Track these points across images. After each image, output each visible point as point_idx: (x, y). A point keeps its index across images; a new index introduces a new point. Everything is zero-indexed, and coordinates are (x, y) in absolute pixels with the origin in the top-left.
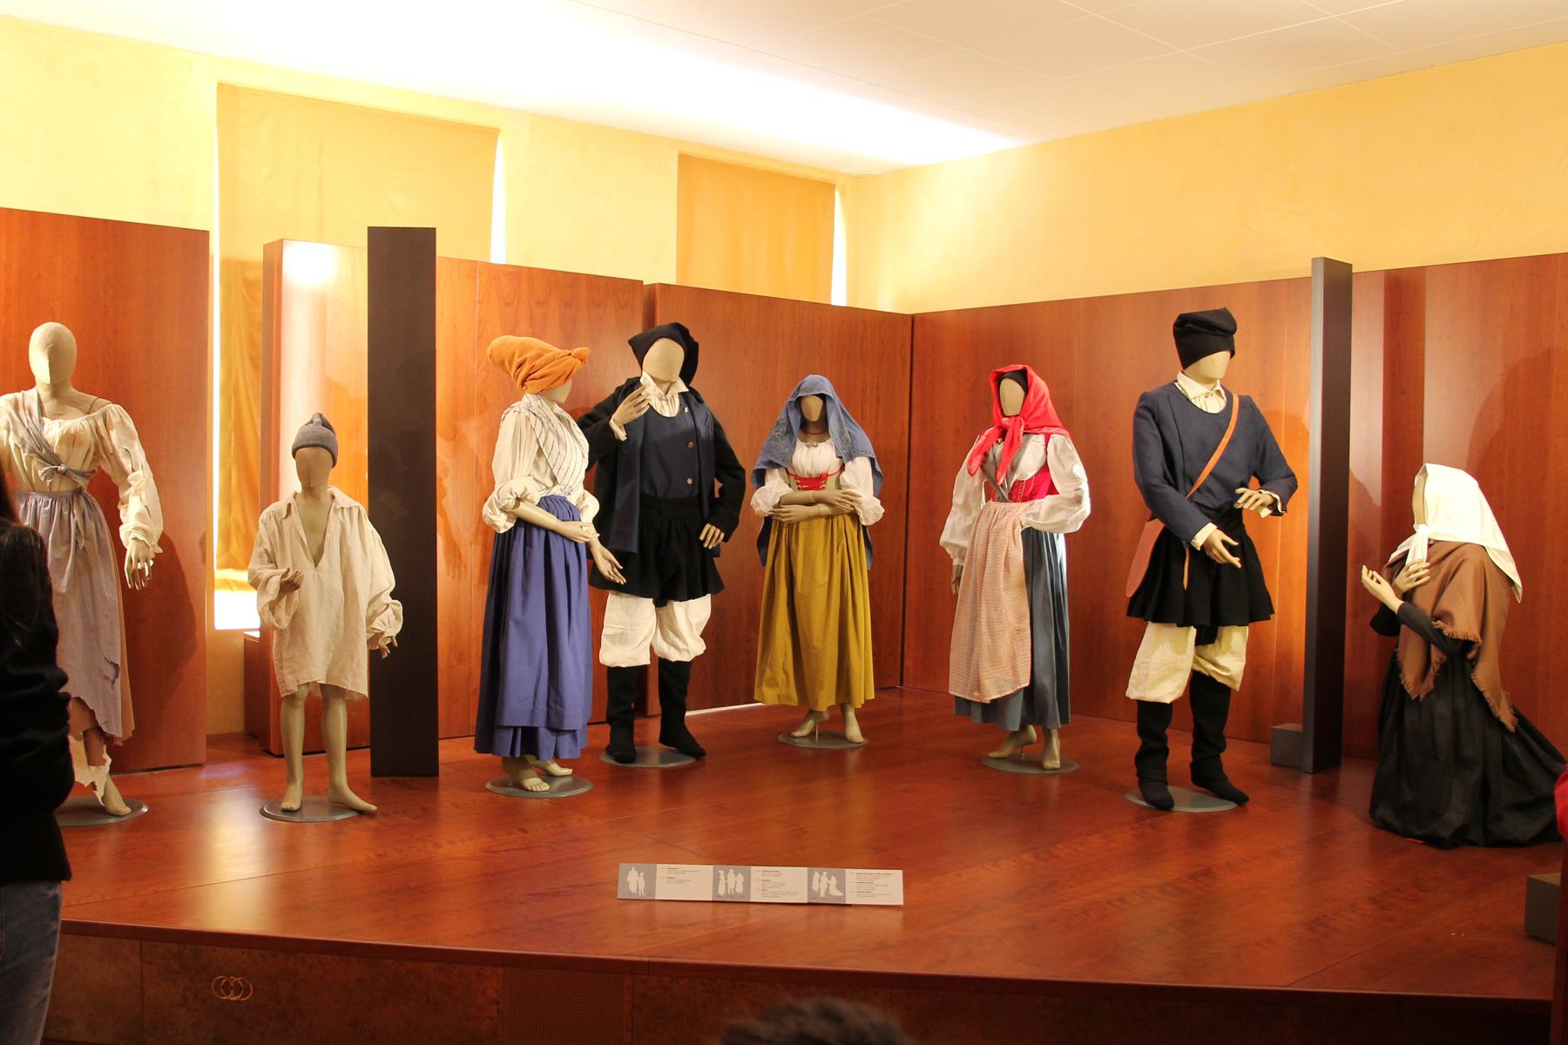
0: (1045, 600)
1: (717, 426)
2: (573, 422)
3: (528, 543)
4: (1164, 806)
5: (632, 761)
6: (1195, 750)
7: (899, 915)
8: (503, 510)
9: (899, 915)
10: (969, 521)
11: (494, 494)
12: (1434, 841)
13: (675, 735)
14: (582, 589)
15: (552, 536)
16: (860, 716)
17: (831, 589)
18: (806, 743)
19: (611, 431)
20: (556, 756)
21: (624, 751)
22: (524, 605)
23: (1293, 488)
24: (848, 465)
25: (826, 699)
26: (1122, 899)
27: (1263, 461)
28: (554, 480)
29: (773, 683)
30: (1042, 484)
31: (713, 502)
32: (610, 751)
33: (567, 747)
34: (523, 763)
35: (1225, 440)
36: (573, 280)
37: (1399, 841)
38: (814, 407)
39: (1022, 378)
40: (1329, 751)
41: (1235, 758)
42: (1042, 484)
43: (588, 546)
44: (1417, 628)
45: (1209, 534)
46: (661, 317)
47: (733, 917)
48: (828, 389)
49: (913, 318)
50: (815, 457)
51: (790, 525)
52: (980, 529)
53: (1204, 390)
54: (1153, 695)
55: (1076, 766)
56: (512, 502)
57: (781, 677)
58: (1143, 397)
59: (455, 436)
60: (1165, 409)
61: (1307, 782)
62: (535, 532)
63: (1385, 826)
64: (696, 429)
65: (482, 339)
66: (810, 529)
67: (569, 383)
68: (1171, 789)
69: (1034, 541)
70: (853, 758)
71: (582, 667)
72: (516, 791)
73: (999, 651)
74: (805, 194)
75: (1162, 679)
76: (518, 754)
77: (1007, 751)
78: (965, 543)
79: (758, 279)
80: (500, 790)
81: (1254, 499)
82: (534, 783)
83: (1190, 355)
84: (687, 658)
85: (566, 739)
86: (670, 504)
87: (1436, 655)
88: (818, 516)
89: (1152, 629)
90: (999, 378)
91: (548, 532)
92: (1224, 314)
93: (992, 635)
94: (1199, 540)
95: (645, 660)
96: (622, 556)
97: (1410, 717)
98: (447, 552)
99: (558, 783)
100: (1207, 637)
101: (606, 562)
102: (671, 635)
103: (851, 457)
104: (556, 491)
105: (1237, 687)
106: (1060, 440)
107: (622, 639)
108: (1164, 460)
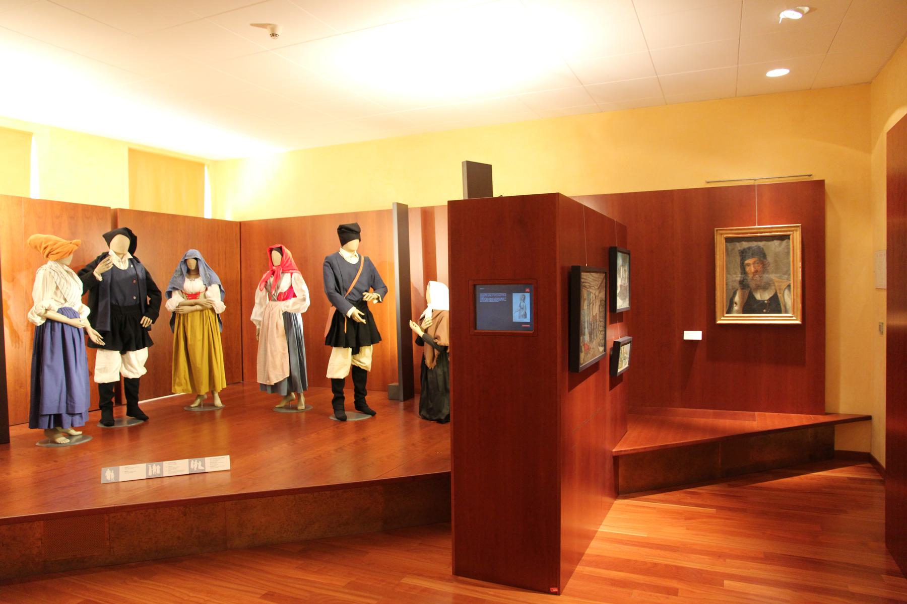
0: (294, 341)
1: (147, 273)
2: (74, 273)
3: (53, 329)
4: (343, 419)
5: (113, 425)
6: (356, 396)
7: (229, 473)
8: (39, 315)
9: (229, 473)
10: (262, 310)
11: (34, 308)
12: (440, 421)
13: (134, 411)
14: (82, 348)
15: (65, 326)
16: (221, 396)
17: (205, 344)
18: (197, 409)
19: (94, 277)
20: (72, 425)
21: (108, 421)
22: (52, 358)
23: (386, 292)
24: (209, 288)
25: (204, 389)
26: (320, 456)
27: (374, 282)
28: (65, 300)
29: (180, 384)
30: (290, 294)
31: (147, 306)
32: (102, 422)
33: (78, 421)
34: (55, 431)
35: (359, 274)
36: (74, 207)
37: (428, 422)
38: (192, 264)
39: (280, 250)
40: (408, 393)
41: (372, 398)
42: (290, 294)
43: (85, 330)
44: (429, 343)
45: (353, 311)
46: (121, 226)
47: (156, 484)
48: (199, 256)
49: (240, 223)
50: (193, 285)
51: (184, 315)
52: (266, 313)
53: (350, 254)
54: (336, 376)
55: (312, 407)
56: (43, 311)
57: (183, 381)
58: (327, 258)
59: (13, 280)
60: (335, 262)
61: (402, 405)
62: (56, 324)
63: (424, 418)
64: (137, 275)
65: (26, 234)
66: (193, 316)
67: (71, 256)
68: (347, 413)
69: (288, 317)
70: (218, 414)
71: (84, 385)
72: (53, 445)
73: (276, 363)
74: (193, 169)
75: (339, 369)
76: (52, 427)
77: (283, 404)
78: (260, 319)
79: (169, 208)
80: (44, 445)
81: (370, 297)
82: (61, 439)
83: (344, 242)
84: (138, 377)
85: (77, 418)
86: (124, 309)
87: (436, 352)
88: (197, 311)
89: (334, 349)
90: (271, 250)
91: (63, 324)
92: (356, 225)
93: (272, 356)
94: (349, 314)
95: (118, 379)
96: (103, 333)
97: (430, 376)
98: (11, 336)
99: (74, 439)
100: (356, 352)
101: (95, 336)
102: (129, 367)
103: (210, 284)
104: (67, 305)
105: (369, 370)
106: (298, 276)
107: (104, 370)
108: (333, 282)
